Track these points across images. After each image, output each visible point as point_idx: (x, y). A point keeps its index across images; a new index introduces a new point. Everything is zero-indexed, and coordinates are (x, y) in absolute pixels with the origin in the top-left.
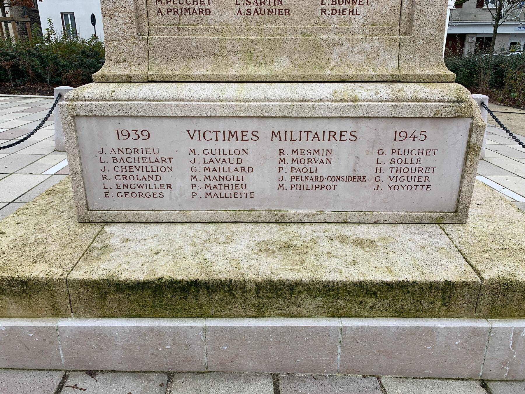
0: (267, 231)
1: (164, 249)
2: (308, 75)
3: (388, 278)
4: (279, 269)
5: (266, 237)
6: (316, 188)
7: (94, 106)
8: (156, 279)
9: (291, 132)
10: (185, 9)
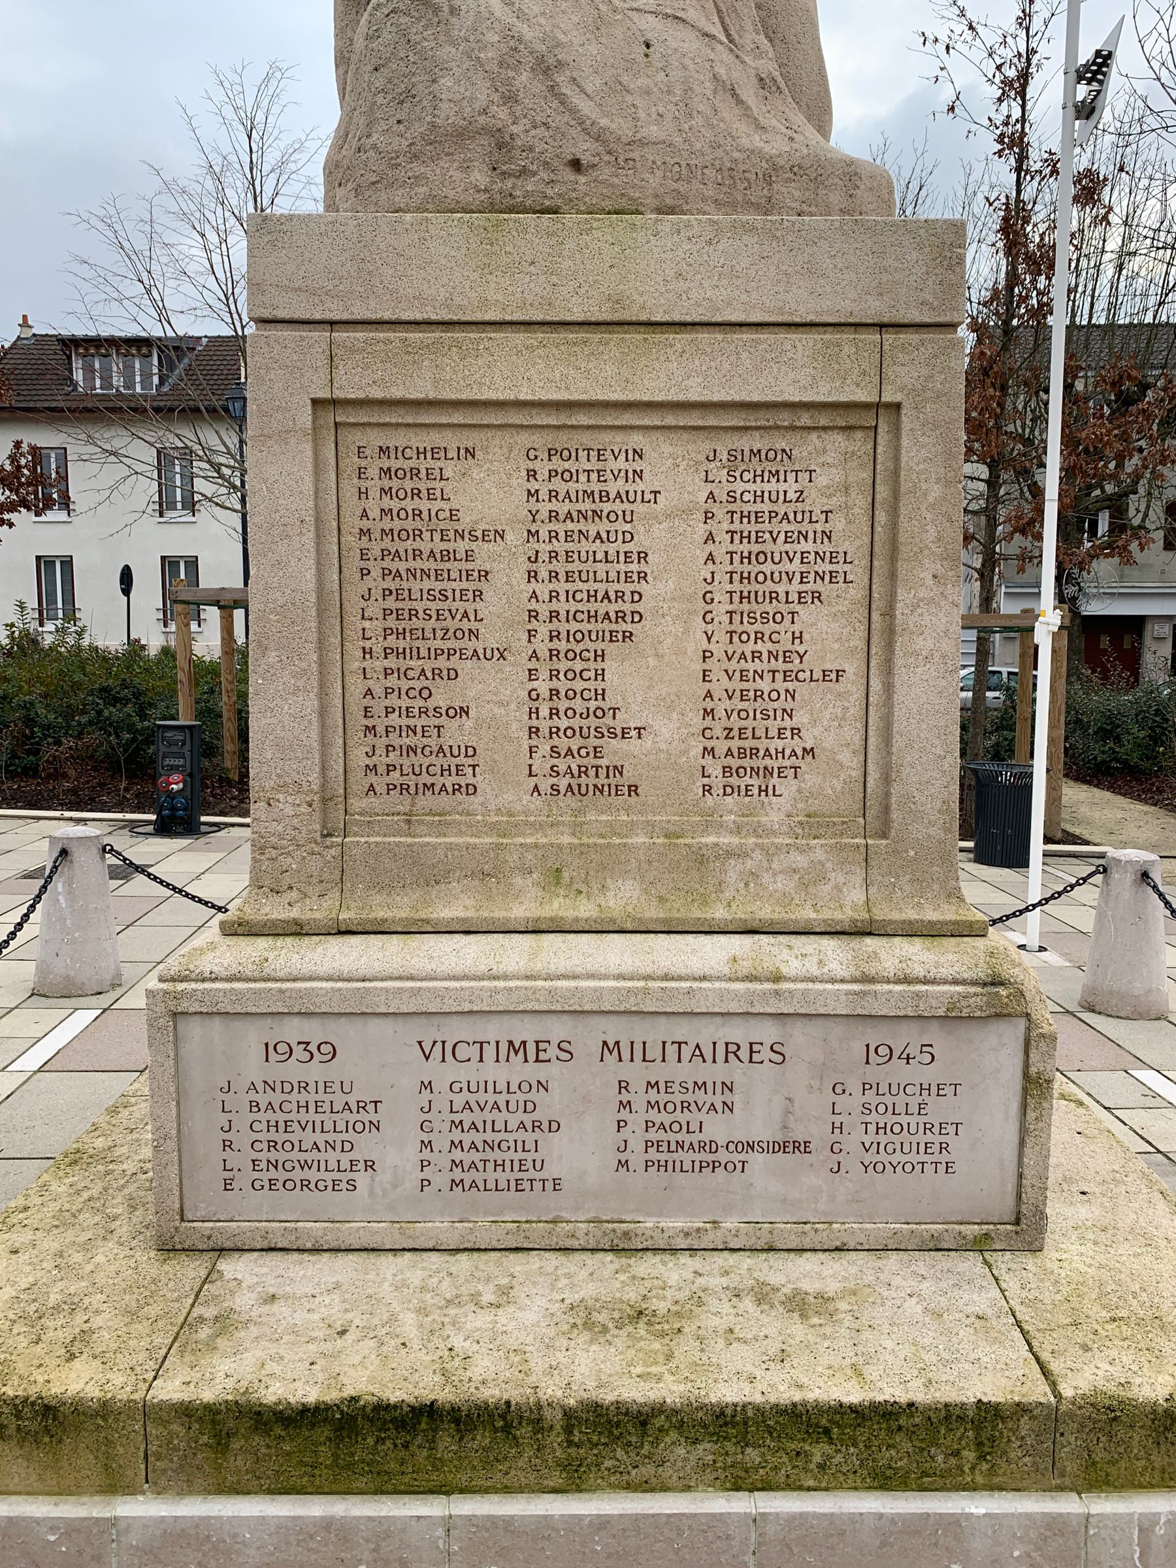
0: (591, 1274)
1: (357, 1322)
2: (678, 919)
3: (853, 1395)
4: (617, 1373)
5: (588, 1291)
7: (221, 994)
8: (343, 1400)
9: (644, 1043)
10: (425, 785)
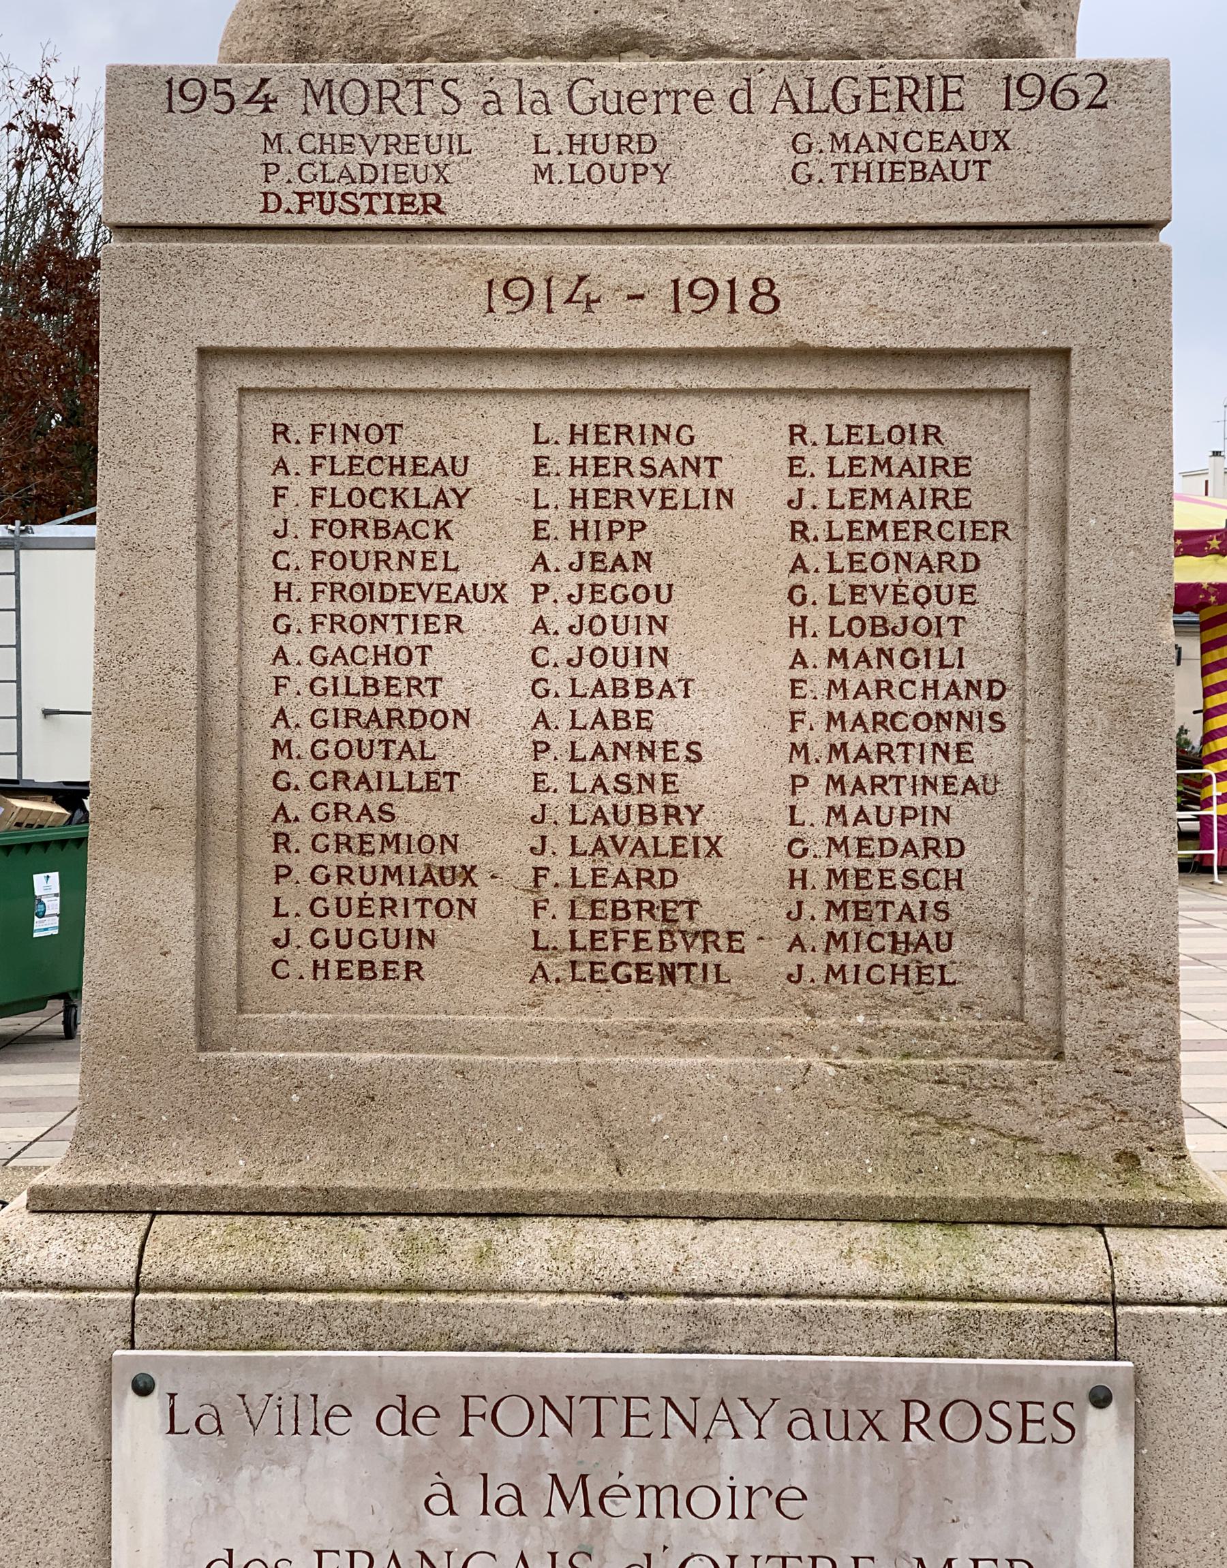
6: (611, 531)
